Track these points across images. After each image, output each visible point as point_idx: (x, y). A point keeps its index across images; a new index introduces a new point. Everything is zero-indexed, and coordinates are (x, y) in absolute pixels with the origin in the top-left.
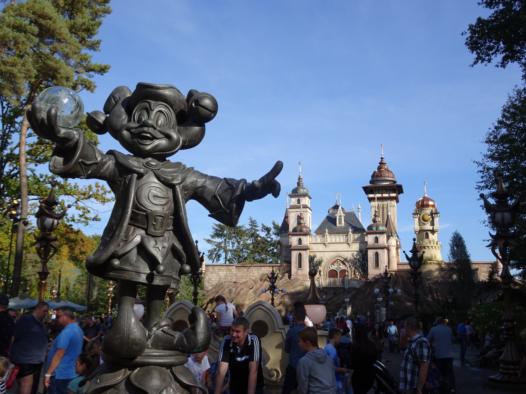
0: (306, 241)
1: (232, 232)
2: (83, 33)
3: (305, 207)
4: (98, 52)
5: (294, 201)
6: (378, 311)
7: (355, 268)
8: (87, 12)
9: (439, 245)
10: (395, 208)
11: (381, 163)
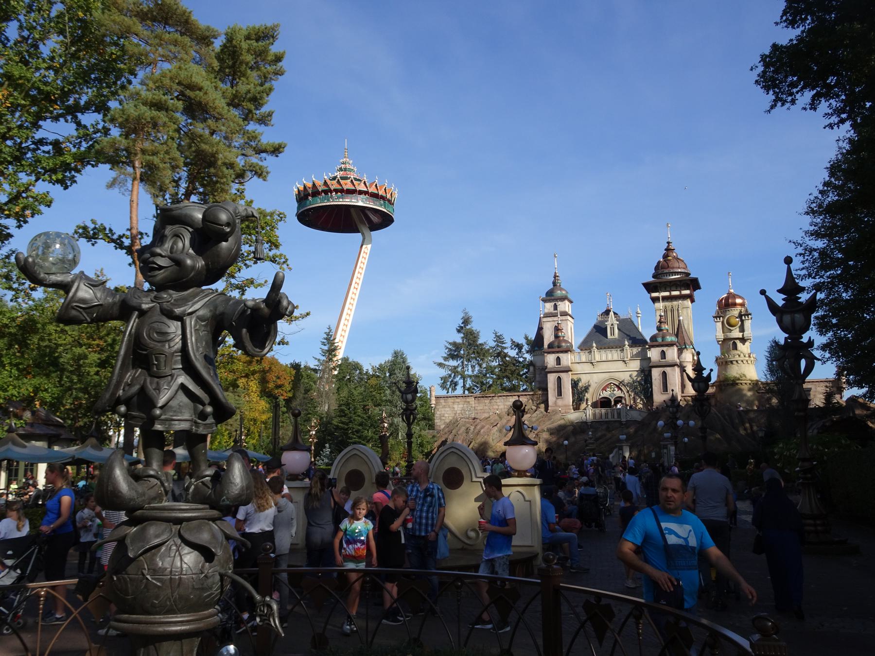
0: (567, 359)
1: (471, 352)
2: (248, 104)
3: (564, 314)
4: (270, 127)
5: (549, 307)
6: (665, 451)
7: (635, 393)
8: (253, 75)
9: (752, 359)
10: (690, 311)
11: (668, 249)
